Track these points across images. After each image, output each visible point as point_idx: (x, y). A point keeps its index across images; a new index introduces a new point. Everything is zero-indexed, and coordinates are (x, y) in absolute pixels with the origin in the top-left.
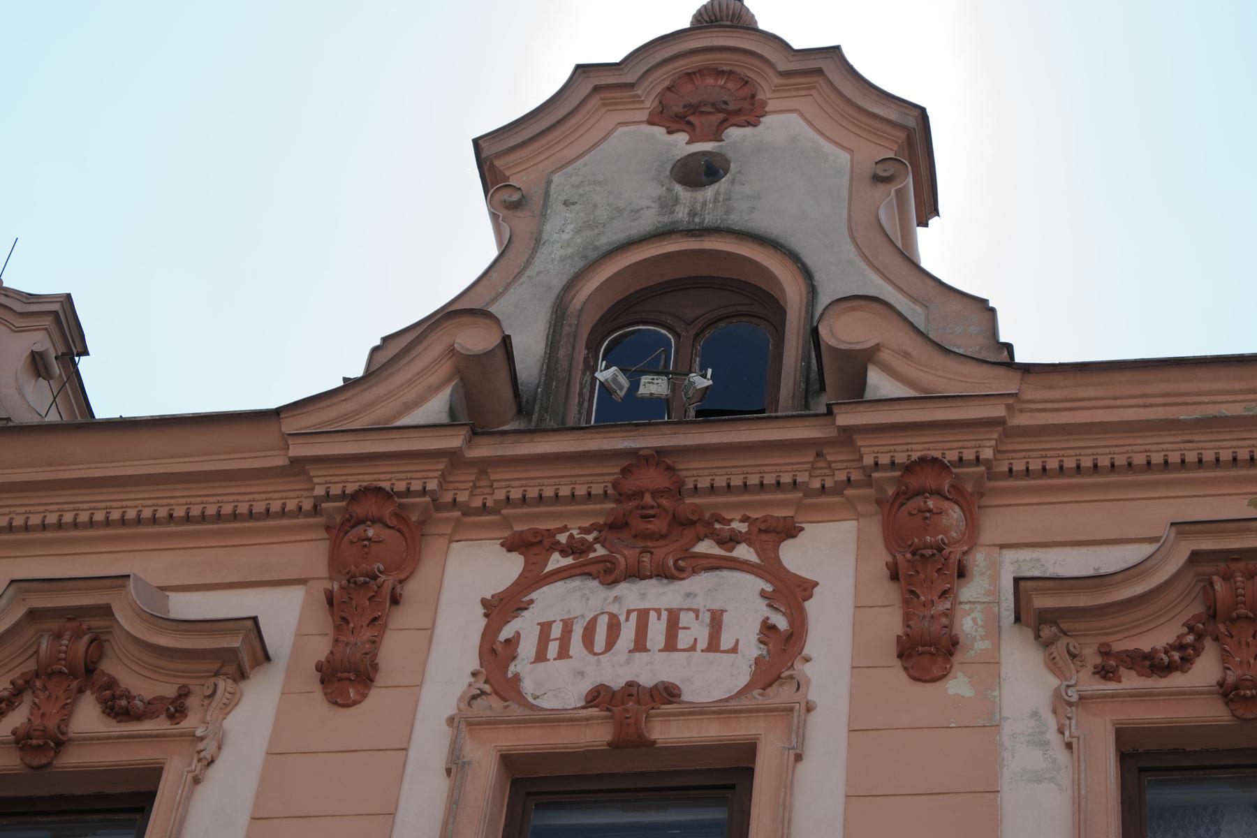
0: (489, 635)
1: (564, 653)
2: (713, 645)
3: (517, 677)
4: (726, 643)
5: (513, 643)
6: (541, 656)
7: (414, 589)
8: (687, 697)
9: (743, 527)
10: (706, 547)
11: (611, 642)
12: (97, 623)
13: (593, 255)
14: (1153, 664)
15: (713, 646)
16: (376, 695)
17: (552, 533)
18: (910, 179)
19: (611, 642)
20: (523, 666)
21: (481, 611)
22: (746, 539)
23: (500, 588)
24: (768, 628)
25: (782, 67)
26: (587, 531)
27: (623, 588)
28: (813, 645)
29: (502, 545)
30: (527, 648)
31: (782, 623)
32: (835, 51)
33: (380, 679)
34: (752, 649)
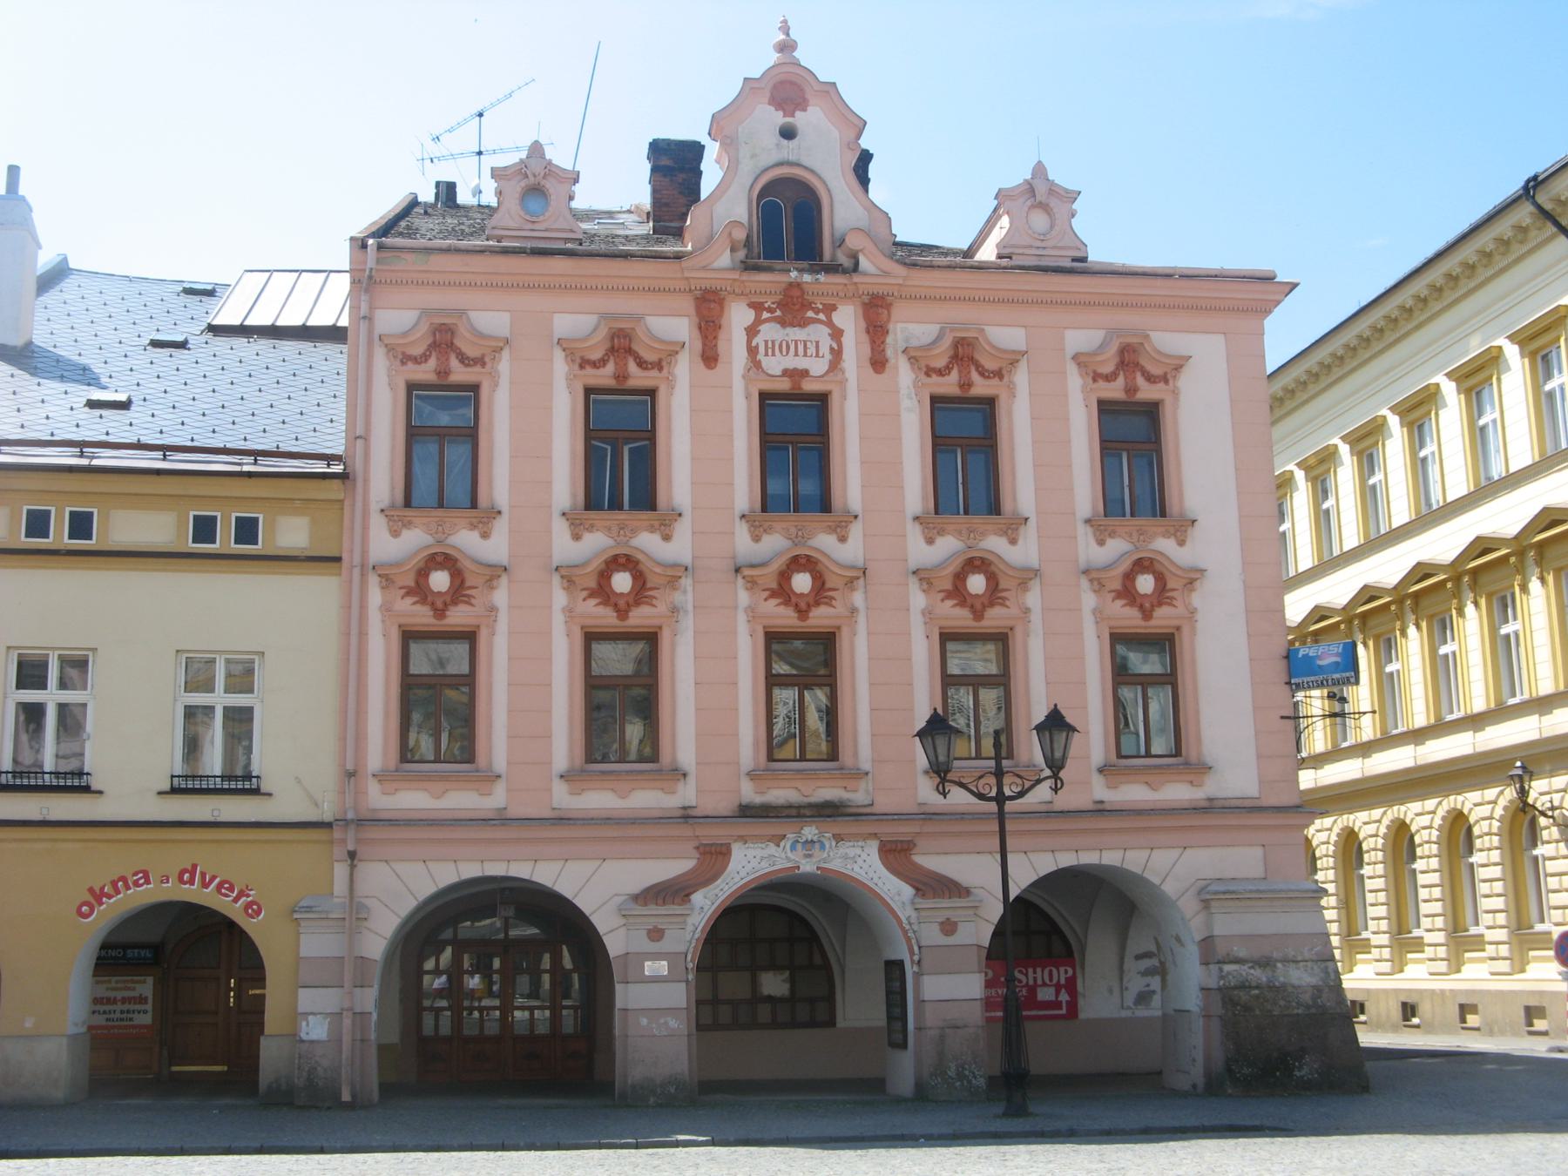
0: (749, 342)
1: (773, 355)
2: (817, 356)
3: (760, 361)
4: (821, 355)
5: (757, 347)
6: (766, 355)
7: (724, 322)
8: (811, 374)
9: (821, 307)
10: (810, 314)
11: (787, 353)
12: (1353, 680)
13: (758, 172)
14: (940, 373)
15: (817, 356)
16: (719, 365)
17: (762, 303)
18: (1389, 599)
19: (780, 346)
20: (760, 356)
21: (745, 333)
22: (822, 311)
23: (749, 324)
24: (832, 349)
25: (815, 88)
26: (773, 303)
27: (789, 330)
28: (845, 356)
29: (748, 305)
30: (762, 349)
31: (836, 347)
32: (834, 84)
33: (720, 360)
34: (828, 356)
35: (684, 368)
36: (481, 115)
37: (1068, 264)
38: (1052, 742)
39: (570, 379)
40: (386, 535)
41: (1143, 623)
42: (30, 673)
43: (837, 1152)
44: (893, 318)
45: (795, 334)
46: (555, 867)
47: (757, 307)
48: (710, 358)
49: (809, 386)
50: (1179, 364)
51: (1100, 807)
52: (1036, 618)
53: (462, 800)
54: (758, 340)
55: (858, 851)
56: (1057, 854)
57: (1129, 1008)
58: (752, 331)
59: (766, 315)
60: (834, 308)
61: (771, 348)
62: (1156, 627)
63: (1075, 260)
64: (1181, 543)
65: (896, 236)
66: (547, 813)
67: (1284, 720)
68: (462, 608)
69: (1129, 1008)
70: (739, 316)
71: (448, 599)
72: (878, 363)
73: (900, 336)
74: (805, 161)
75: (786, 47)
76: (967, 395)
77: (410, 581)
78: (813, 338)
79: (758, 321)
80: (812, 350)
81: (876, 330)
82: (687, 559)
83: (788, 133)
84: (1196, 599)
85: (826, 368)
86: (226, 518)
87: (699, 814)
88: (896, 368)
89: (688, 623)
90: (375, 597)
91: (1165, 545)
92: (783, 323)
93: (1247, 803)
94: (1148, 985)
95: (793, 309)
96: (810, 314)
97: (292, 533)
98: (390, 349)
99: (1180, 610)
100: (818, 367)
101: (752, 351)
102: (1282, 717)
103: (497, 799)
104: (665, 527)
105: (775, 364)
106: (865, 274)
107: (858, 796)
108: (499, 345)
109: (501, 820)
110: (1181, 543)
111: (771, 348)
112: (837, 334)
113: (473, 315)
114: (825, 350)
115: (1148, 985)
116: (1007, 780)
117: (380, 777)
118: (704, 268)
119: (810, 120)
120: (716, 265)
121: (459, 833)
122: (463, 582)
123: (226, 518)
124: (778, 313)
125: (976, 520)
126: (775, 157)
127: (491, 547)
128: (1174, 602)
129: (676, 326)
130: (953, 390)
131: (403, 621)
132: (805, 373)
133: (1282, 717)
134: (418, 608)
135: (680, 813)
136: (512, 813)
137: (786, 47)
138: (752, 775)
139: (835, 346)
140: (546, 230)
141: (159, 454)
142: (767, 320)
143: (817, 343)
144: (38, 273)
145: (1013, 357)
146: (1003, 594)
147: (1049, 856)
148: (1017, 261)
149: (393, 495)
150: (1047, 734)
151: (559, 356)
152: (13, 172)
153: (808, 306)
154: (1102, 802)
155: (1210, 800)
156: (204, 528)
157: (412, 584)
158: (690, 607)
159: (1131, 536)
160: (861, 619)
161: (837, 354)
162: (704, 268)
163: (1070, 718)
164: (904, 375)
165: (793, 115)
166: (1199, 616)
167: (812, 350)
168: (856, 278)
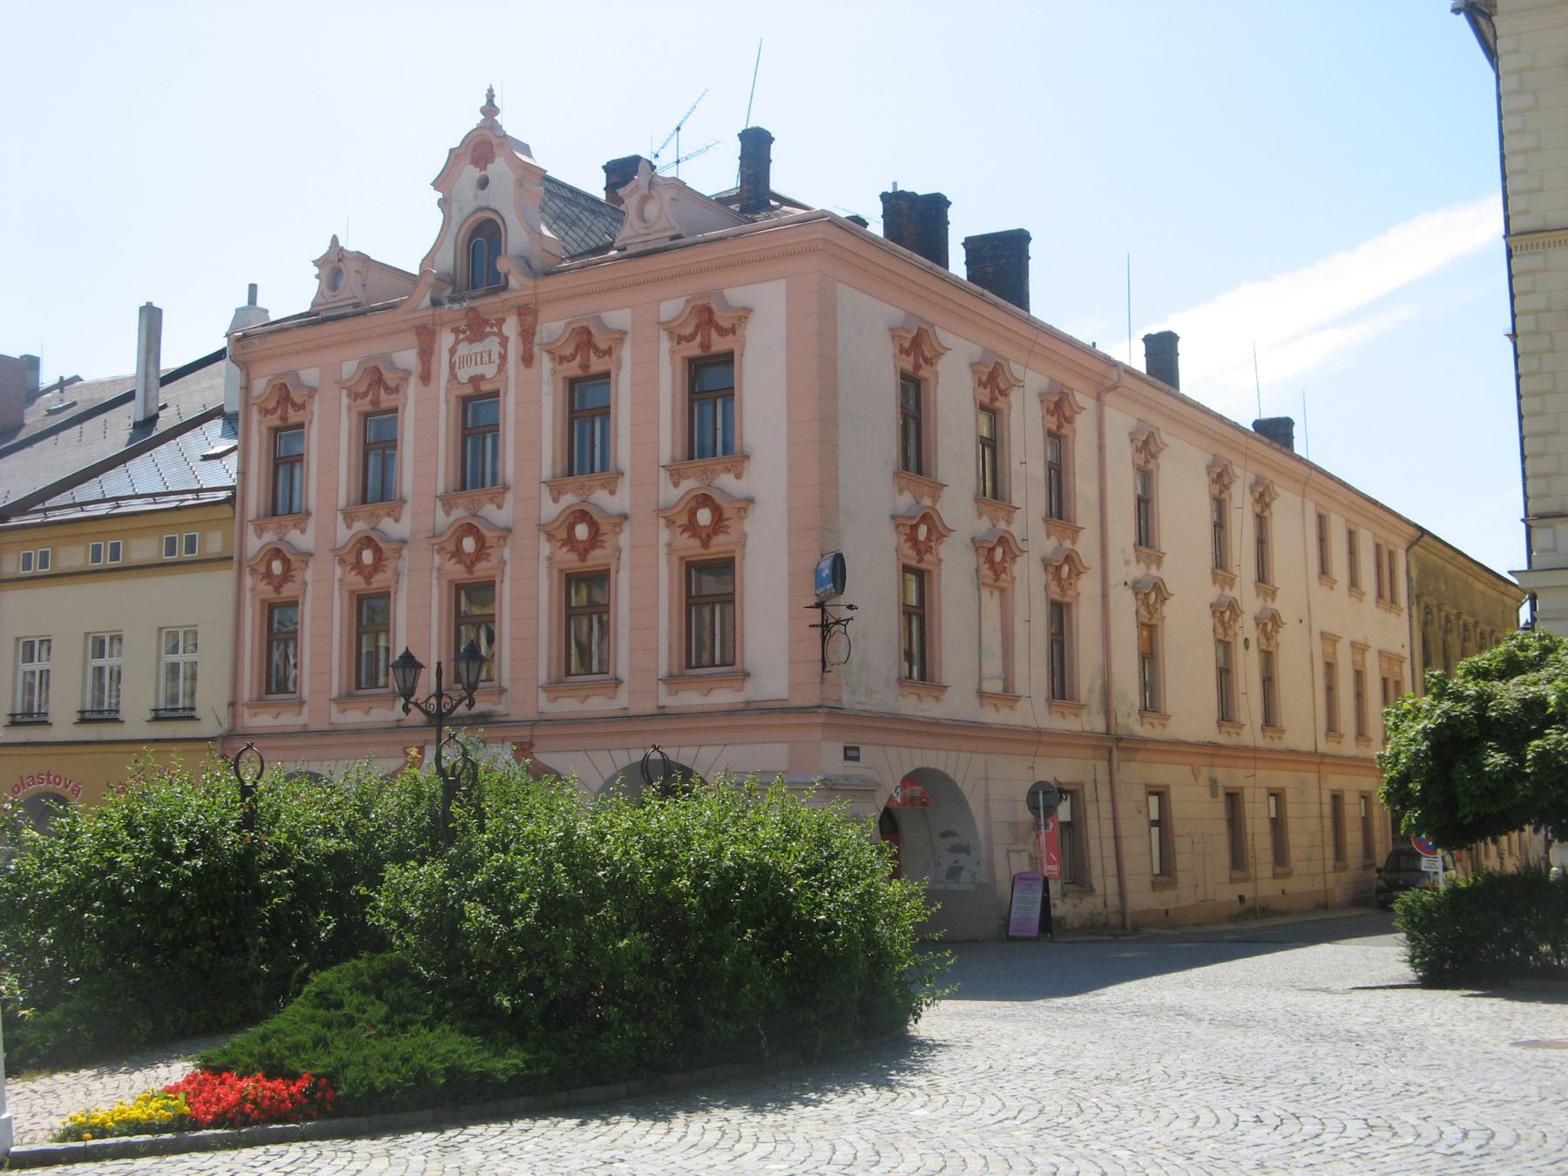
2: (490, 362)
10: (488, 329)
15: (490, 362)
24: (500, 353)
34: (497, 361)
35: (412, 388)
36: (678, 129)
37: (350, 310)
38: (468, 668)
39: (673, 353)
40: (254, 536)
41: (702, 551)
42: (29, 650)
43: (1035, 1002)
44: (540, 320)
45: (478, 347)
46: (691, 751)
47: (456, 331)
48: (426, 378)
49: (486, 387)
50: (745, 314)
51: (661, 711)
52: (625, 555)
53: (598, 704)
54: (456, 357)
55: (499, 750)
56: (631, 751)
57: (941, 881)
58: (453, 351)
59: (461, 336)
60: (503, 320)
61: (467, 360)
62: (714, 554)
63: (673, 238)
64: (738, 476)
65: (266, 311)
66: (327, 727)
67: (813, 629)
68: (290, 584)
69: (941, 881)
70: (446, 339)
71: (587, 545)
72: (527, 359)
73: (544, 334)
74: (492, 205)
75: (490, 110)
76: (710, 354)
77: (684, 520)
78: (487, 349)
79: (457, 342)
80: (486, 359)
81: (527, 334)
82: (626, 508)
83: (484, 183)
84: (748, 526)
85: (496, 370)
86: (180, 537)
87: (404, 725)
88: (541, 361)
89: (404, 583)
90: (249, 581)
91: (726, 481)
92: (471, 341)
93: (777, 705)
94: (957, 861)
95: (476, 328)
96: (488, 329)
97: (214, 543)
98: (671, 333)
99: (609, 551)
100: (490, 371)
101: (452, 366)
102: (811, 626)
103: (622, 700)
104: (611, 485)
105: (464, 374)
106: (513, 290)
107: (500, 708)
108: (313, 391)
109: (305, 732)
110: (738, 476)
111: (467, 360)
112: (504, 342)
113: (728, 293)
114: (495, 356)
115: (957, 861)
116: (444, 700)
117: (250, 705)
118: (414, 310)
119: (498, 169)
120: (421, 306)
121: (767, 720)
122: (721, 515)
123: (180, 537)
124: (468, 333)
125: (584, 479)
126: (473, 206)
127: (500, 515)
128: (605, 545)
129: (408, 358)
130: (577, 372)
131: (683, 554)
132: (482, 377)
133: (811, 626)
134: (692, 540)
135: (394, 724)
136: (311, 728)
137: (490, 110)
138: (671, 680)
139: (502, 352)
140: (341, 300)
141: (151, 500)
142: (463, 340)
143: (490, 352)
144: (162, 375)
145: (742, 313)
146: (293, 573)
147: (625, 753)
148: (630, 250)
149: (258, 511)
150: (401, 671)
151: (664, 336)
152: (253, 289)
153: (486, 322)
154: (664, 707)
155: (748, 702)
156: (171, 546)
157: (566, 536)
158: (406, 571)
159: (591, 487)
160: (508, 569)
161: (503, 358)
162: (414, 310)
163: (419, 658)
164: (545, 364)
165: (485, 169)
166: (750, 542)
167: (486, 359)
168: (505, 296)
